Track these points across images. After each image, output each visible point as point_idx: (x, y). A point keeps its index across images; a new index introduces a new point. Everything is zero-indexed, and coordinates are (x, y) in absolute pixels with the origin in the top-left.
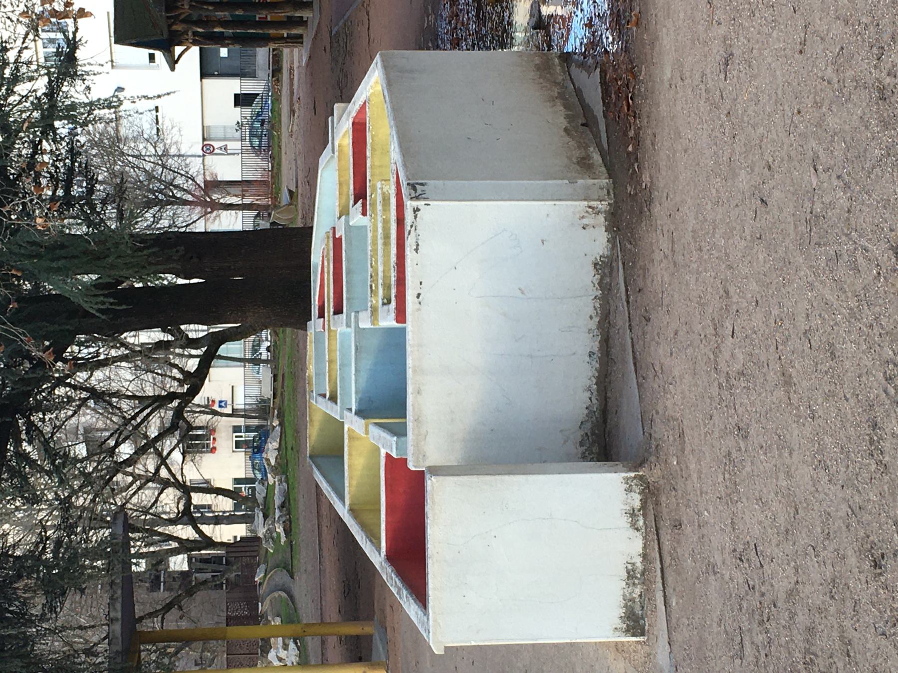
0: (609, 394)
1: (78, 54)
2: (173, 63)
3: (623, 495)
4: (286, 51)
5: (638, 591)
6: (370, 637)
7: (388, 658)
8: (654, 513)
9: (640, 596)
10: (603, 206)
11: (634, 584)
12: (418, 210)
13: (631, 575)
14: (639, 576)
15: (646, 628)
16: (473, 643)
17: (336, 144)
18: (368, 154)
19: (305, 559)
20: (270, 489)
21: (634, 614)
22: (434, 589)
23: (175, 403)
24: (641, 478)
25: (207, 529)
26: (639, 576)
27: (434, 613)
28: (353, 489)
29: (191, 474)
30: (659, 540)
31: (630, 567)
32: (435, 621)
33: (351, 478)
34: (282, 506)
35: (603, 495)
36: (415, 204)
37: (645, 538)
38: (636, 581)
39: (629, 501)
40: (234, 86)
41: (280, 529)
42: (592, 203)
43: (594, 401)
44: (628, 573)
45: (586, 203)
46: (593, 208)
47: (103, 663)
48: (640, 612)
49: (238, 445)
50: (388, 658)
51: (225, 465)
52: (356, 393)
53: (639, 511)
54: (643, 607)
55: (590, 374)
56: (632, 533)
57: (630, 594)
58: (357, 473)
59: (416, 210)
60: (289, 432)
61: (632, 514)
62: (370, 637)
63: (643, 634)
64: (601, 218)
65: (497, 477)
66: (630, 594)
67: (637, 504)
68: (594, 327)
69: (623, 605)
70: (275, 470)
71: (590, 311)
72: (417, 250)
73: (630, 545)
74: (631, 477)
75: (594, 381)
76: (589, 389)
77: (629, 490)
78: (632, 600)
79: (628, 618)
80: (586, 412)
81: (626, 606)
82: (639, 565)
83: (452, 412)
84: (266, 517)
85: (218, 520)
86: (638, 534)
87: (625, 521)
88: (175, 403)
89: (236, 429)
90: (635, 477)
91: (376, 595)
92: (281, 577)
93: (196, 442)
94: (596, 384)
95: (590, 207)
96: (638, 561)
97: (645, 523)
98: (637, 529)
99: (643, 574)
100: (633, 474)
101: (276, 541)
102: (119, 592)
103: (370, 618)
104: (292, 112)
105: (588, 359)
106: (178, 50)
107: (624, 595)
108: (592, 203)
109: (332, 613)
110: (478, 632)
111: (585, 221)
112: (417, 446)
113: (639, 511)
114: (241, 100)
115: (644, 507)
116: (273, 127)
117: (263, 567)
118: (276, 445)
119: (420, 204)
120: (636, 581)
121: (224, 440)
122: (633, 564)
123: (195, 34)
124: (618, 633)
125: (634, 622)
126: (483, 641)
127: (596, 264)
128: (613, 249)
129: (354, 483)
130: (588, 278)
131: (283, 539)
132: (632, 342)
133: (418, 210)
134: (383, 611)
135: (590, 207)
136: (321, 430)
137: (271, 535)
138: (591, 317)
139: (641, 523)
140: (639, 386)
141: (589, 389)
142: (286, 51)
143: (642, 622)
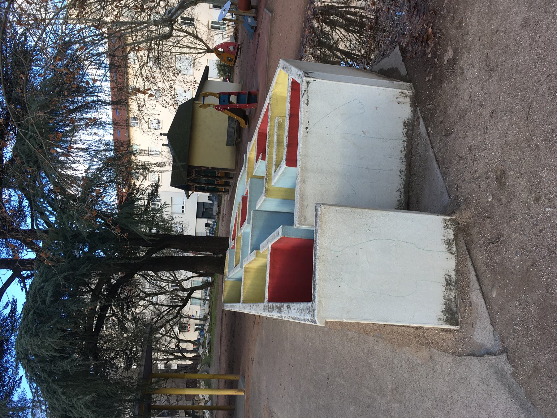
0: (410, 194)
1: (159, 189)
2: (188, 196)
3: (442, 230)
4: (224, 196)
5: (453, 294)
6: (237, 381)
7: (245, 388)
8: (463, 241)
9: (455, 298)
10: (409, 93)
11: (451, 289)
12: (309, 83)
13: (448, 283)
14: (453, 284)
15: (459, 320)
16: (345, 320)
17: (248, 157)
18: (269, 120)
19: (214, 361)
20: (205, 339)
21: (451, 310)
22: (320, 280)
23: (178, 308)
24: (454, 220)
25: (185, 354)
26: (453, 284)
27: (319, 296)
28: (245, 294)
29: (181, 337)
30: (471, 258)
31: (447, 277)
32: (319, 302)
33: (244, 289)
34: (208, 343)
35: (428, 230)
36: (308, 79)
37: (457, 259)
38: (452, 288)
39: (446, 234)
40: (205, 221)
41: (207, 351)
42: (403, 91)
43: (402, 198)
44: (447, 282)
45: (400, 90)
46: (404, 94)
47: (135, 382)
48: (455, 309)
49: (196, 330)
50: (245, 388)
51: (192, 335)
52: (251, 245)
53: (453, 241)
54: (457, 306)
55: (400, 182)
56: (448, 255)
57: (448, 296)
58: (247, 287)
59: (308, 83)
60: (213, 319)
61: (449, 243)
62: (237, 381)
63: (457, 324)
64: (408, 100)
65: (364, 210)
66: (448, 296)
67: (452, 237)
68: (403, 157)
69: (443, 303)
70: (207, 332)
71: (401, 147)
72: (307, 104)
73: (448, 264)
74: (447, 220)
75: (402, 186)
76: (399, 190)
77: (446, 227)
78: (450, 300)
79: (447, 312)
80: (398, 203)
81: (446, 304)
82: (453, 276)
83: (322, 195)
84: (203, 348)
85: (188, 352)
86: (453, 256)
87: (443, 247)
88: (178, 308)
89: (196, 325)
90: (450, 220)
91: (242, 364)
92: (206, 367)
93: (184, 328)
94: (403, 188)
95: (402, 93)
96: (453, 274)
97: (457, 249)
98: (452, 253)
99: (456, 283)
100: (448, 218)
101: (205, 355)
102: (145, 354)
103: (238, 373)
104: (223, 221)
105: (399, 174)
106: (190, 192)
107: (444, 296)
108: (403, 91)
109: (223, 371)
110: (348, 312)
111: (399, 100)
112: (301, 212)
113: (453, 241)
114: (207, 225)
115: (456, 238)
116: (216, 230)
117: (200, 364)
118: (208, 324)
119: (311, 79)
120: (452, 288)
121: (192, 328)
122: (450, 276)
123: (196, 187)
124: (441, 322)
125: (451, 315)
126: (351, 319)
127: (404, 123)
128: (414, 116)
129: (245, 291)
130: (400, 130)
131: (208, 354)
132: (435, 155)
133: (309, 83)
134: (244, 370)
135: (402, 93)
136: (228, 293)
137: (204, 353)
138: (401, 151)
139: (454, 249)
140: (443, 174)
141: (399, 190)
142: (224, 196)
143: (456, 316)
